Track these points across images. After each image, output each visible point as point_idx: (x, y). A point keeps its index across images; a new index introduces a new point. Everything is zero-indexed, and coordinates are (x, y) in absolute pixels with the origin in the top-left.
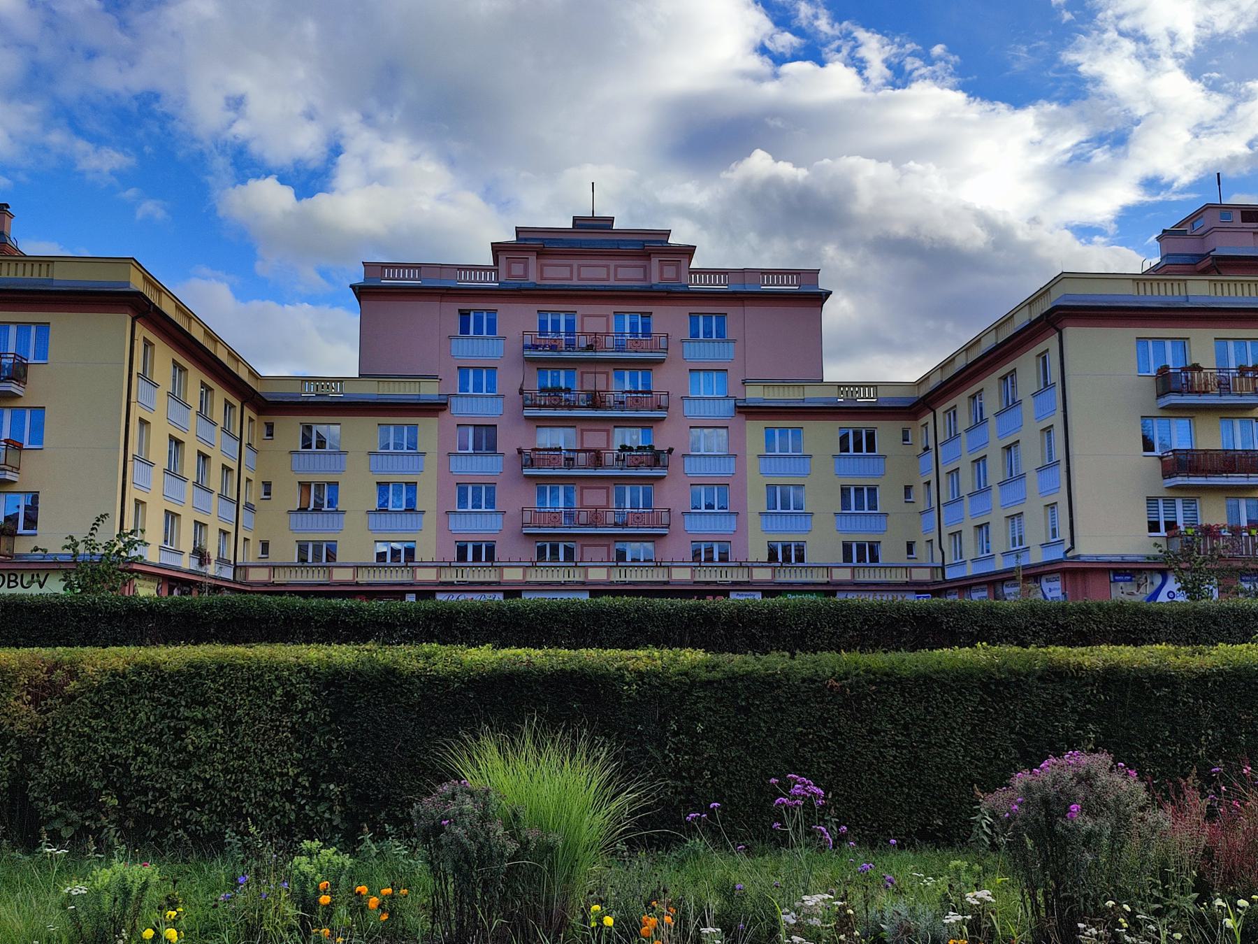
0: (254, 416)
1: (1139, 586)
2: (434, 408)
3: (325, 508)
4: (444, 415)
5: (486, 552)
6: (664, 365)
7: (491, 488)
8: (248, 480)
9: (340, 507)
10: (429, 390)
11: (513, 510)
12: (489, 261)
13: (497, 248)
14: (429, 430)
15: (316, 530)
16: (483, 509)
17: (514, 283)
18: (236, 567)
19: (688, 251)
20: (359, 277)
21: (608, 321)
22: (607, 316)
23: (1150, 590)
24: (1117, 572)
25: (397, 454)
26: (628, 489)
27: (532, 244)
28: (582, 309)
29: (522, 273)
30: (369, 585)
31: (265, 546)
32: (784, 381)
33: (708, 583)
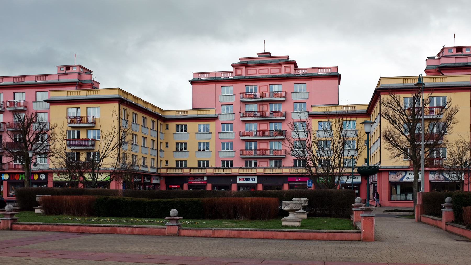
0: (162, 123)
1: (398, 176)
2: (214, 119)
3: (184, 150)
4: (217, 121)
5: (230, 164)
6: (285, 102)
8: (161, 143)
9: (210, 150)
10: (212, 113)
14: (212, 124)
15: (181, 156)
16: (229, 150)
17: (238, 77)
18: (157, 169)
20: (191, 78)
22: (267, 86)
23: (401, 177)
24: (391, 171)
25: (203, 133)
26: (253, 143)
27: (245, 64)
28: (259, 84)
30: (193, 174)
31: (167, 162)
33: (269, 173)
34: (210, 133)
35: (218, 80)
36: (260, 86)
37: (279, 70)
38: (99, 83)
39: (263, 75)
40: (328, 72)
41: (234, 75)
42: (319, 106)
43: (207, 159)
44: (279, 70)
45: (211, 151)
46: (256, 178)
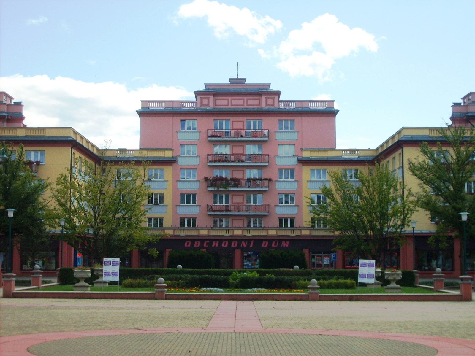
2: (170, 162)
4: (174, 165)
5: (192, 222)
7: (194, 196)
10: (168, 154)
11: (204, 205)
12: (194, 99)
13: (197, 94)
19: (278, 94)
20: (139, 107)
21: (243, 123)
27: (213, 92)
28: (256, 108)
29: (207, 103)
32: (156, 149)
34: (164, 181)
35: (174, 112)
36: (233, 122)
37: (258, 101)
38: (330, 113)
39: (238, 108)
40: (322, 107)
41: (199, 106)
42: (312, 150)
43: (161, 216)
44: (258, 101)
45: (174, 204)
46: (288, 243)
